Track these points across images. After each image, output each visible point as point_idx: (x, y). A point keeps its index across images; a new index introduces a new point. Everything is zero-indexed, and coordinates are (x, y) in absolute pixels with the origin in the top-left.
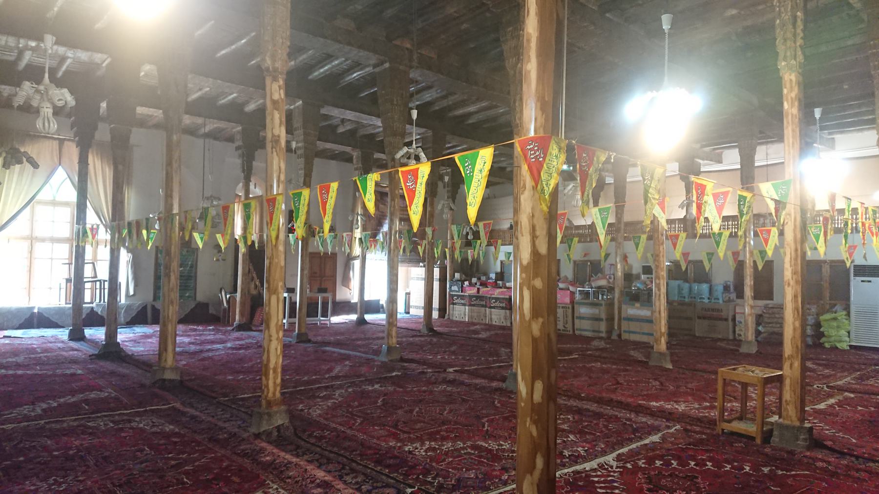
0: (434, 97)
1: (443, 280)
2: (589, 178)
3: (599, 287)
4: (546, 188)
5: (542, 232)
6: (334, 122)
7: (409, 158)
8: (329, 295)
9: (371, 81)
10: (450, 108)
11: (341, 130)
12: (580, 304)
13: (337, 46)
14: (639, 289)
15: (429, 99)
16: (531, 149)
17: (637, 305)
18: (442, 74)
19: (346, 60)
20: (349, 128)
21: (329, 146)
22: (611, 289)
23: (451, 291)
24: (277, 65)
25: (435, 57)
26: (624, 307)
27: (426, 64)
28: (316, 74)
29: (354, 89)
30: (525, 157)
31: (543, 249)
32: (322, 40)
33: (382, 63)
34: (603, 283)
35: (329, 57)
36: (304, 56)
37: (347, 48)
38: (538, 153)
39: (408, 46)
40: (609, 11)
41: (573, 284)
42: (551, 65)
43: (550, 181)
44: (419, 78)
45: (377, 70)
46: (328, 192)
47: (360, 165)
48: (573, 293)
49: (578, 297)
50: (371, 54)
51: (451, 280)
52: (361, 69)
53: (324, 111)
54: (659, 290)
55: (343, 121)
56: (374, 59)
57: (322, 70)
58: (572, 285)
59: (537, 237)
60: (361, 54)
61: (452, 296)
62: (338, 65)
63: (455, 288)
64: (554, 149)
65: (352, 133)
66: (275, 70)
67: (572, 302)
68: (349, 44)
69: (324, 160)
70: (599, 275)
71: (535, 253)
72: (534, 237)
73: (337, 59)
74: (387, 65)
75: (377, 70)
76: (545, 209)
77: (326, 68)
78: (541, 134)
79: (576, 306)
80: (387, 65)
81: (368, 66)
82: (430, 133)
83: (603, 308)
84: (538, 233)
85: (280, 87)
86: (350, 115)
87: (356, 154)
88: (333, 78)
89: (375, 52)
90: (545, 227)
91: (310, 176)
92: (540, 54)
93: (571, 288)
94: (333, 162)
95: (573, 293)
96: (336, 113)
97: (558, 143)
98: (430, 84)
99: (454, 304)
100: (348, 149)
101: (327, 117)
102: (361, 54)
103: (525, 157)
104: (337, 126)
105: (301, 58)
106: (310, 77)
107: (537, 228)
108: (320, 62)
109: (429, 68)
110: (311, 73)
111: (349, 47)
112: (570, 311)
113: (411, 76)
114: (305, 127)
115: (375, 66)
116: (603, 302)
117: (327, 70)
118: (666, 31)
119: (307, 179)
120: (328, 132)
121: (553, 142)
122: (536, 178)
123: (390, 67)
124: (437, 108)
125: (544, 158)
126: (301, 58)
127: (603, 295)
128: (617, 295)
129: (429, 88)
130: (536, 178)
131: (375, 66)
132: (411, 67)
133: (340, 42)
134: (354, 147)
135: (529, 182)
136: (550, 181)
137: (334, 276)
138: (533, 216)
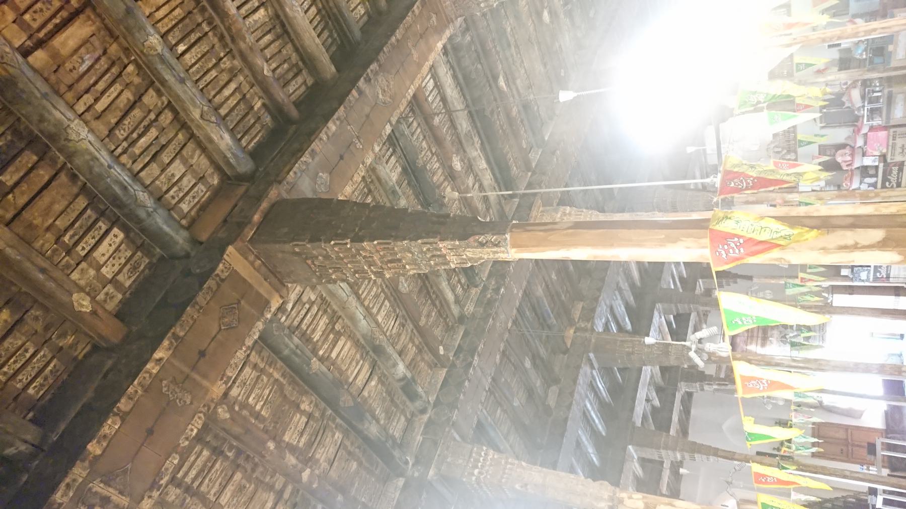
0: (621, 302)
1: (851, 290)
2: (762, 175)
3: (863, 97)
4: (783, 234)
5: (849, 237)
6: (649, 409)
7: (703, 350)
8: (879, 442)
9: (607, 372)
10: (632, 286)
11: (657, 403)
12: (888, 118)
13: (574, 407)
14: (866, 50)
15: (623, 309)
16: (727, 252)
17: (891, 48)
18: (599, 296)
19: (587, 397)
20: (654, 394)
21: (675, 418)
22: (865, 83)
23: (868, 280)
24: (606, 497)
25: (582, 303)
26: (893, 64)
27: (589, 314)
28: (600, 427)
29: (615, 390)
30: (737, 259)
31: (877, 235)
32: (569, 423)
33: (590, 360)
34: (856, 94)
35: (585, 415)
36: (584, 439)
37: (576, 396)
38: (733, 245)
39: (572, 331)
40: (543, 138)
41: (857, 131)
42: (624, 233)
43: (774, 230)
44: (603, 320)
45: (596, 365)
46: (764, 476)
47: (698, 384)
48: (872, 128)
49: (877, 122)
50: (581, 371)
51: (852, 280)
52: (595, 380)
53: (638, 423)
54: (875, 30)
55: (648, 400)
56: (585, 369)
57: (597, 421)
58: (859, 130)
59: (857, 243)
60: (581, 382)
61: (876, 279)
62: (591, 404)
63: (863, 275)
64: (726, 227)
65: (659, 390)
66: (611, 499)
67: (885, 128)
68: (572, 394)
69: (691, 422)
70: (844, 99)
71: (882, 245)
72: (856, 247)
73: (585, 406)
74: (592, 355)
75: (596, 365)
76: (815, 232)
77: (594, 416)
78: (707, 241)
79: (892, 123)
80: (592, 355)
81: (592, 373)
82: (659, 306)
83: (895, 90)
84: (850, 242)
85: (630, 498)
86: (642, 394)
87: (683, 387)
88: (603, 407)
89: (578, 367)
90: (840, 233)
91: (717, 449)
92: (610, 243)
93: (865, 130)
94: (693, 412)
95: (872, 128)
96: (640, 408)
97: (719, 221)
98: (608, 310)
99: (888, 277)
100: (678, 397)
101: (644, 417)
102: (581, 382)
103: (737, 259)
104: (653, 407)
105: (586, 443)
106: (604, 434)
107: (842, 243)
108: (588, 421)
109: (593, 310)
110: (600, 432)
111: (576, 394)
112: (899, 130)
113: (601, 330)
114: (658, 448)
115: (592, 367)
116: (886, 91)
117: (597, 416)
118: (575, 94)
119: (720, 453)
120: (660, 418)
121: (717, 227)
122: (769, 246)
123: (594, 352)
124: (632, 298)
125: (739, 237)
126: (586, 443)
127: (874, 92)
128: (875, 75)
129: (612, 309)
130: (769, 246)
131: (592, 367)
132: (593, 330)
133: (571, 404)
134: (676, 389)
135: (775, 254)
136: (774, 230)
137: (847, 428)
138: (823, 249)
